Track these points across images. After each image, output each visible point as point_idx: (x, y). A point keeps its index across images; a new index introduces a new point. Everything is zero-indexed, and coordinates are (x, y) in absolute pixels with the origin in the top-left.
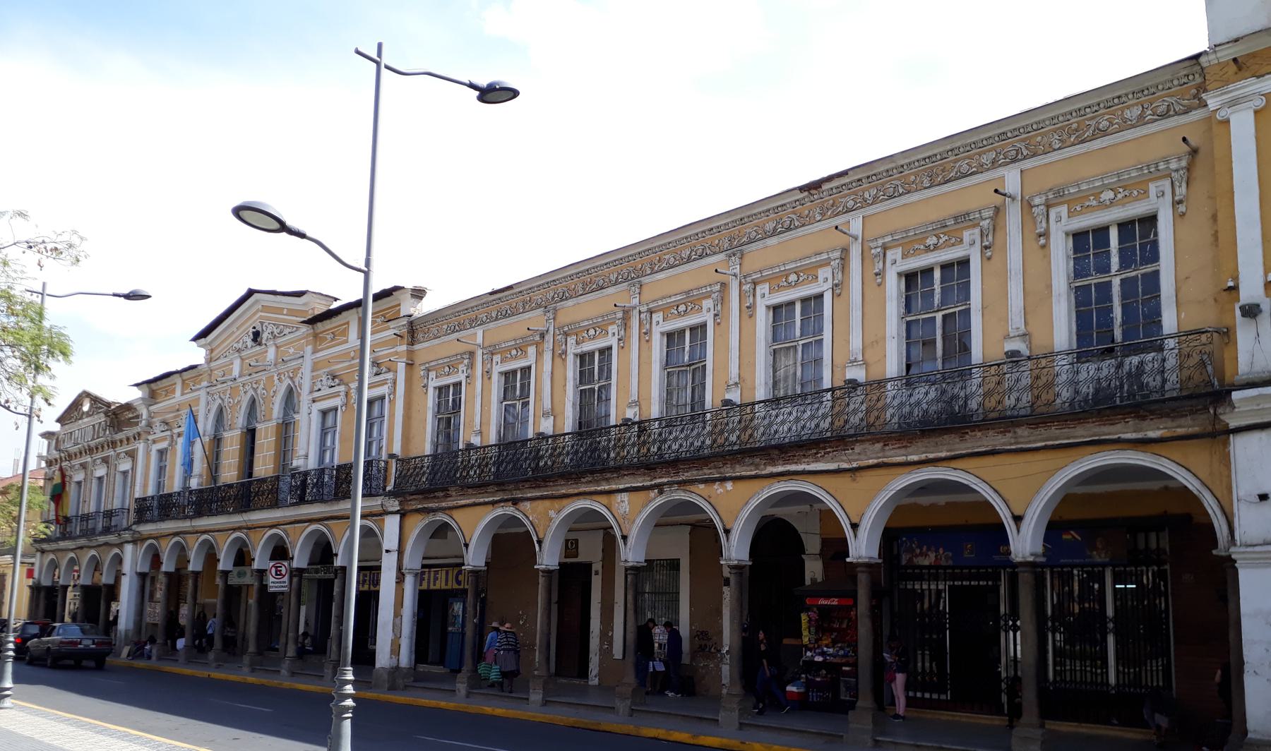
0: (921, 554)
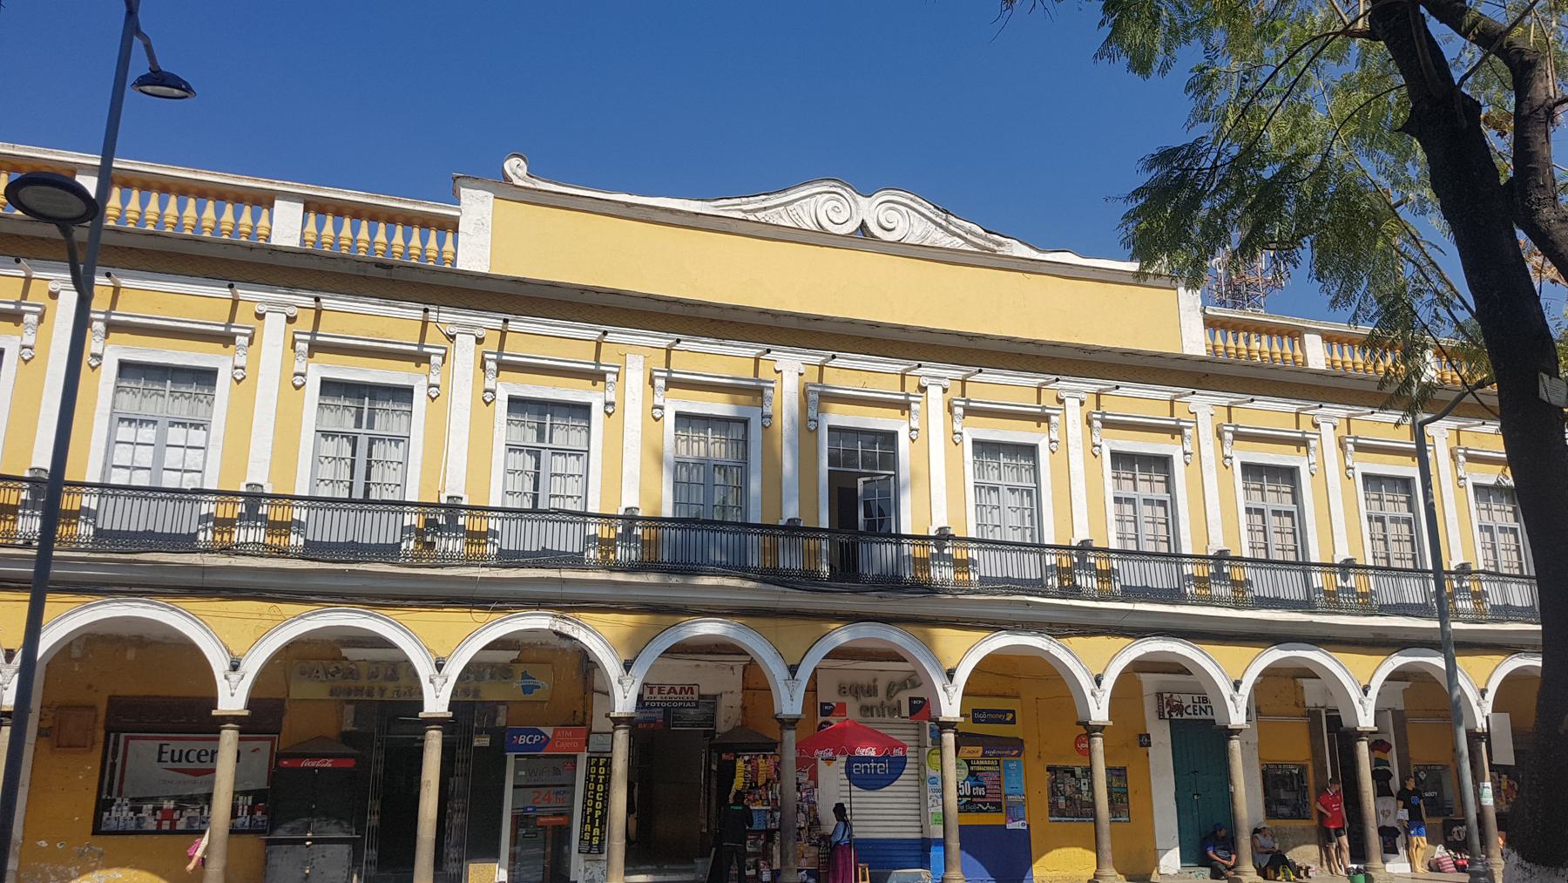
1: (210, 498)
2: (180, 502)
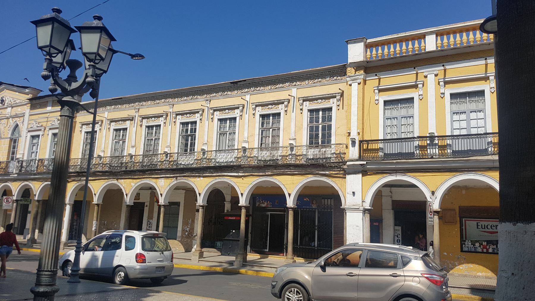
0: (262, 203)
1: (491, 136)
2: (480, 138)
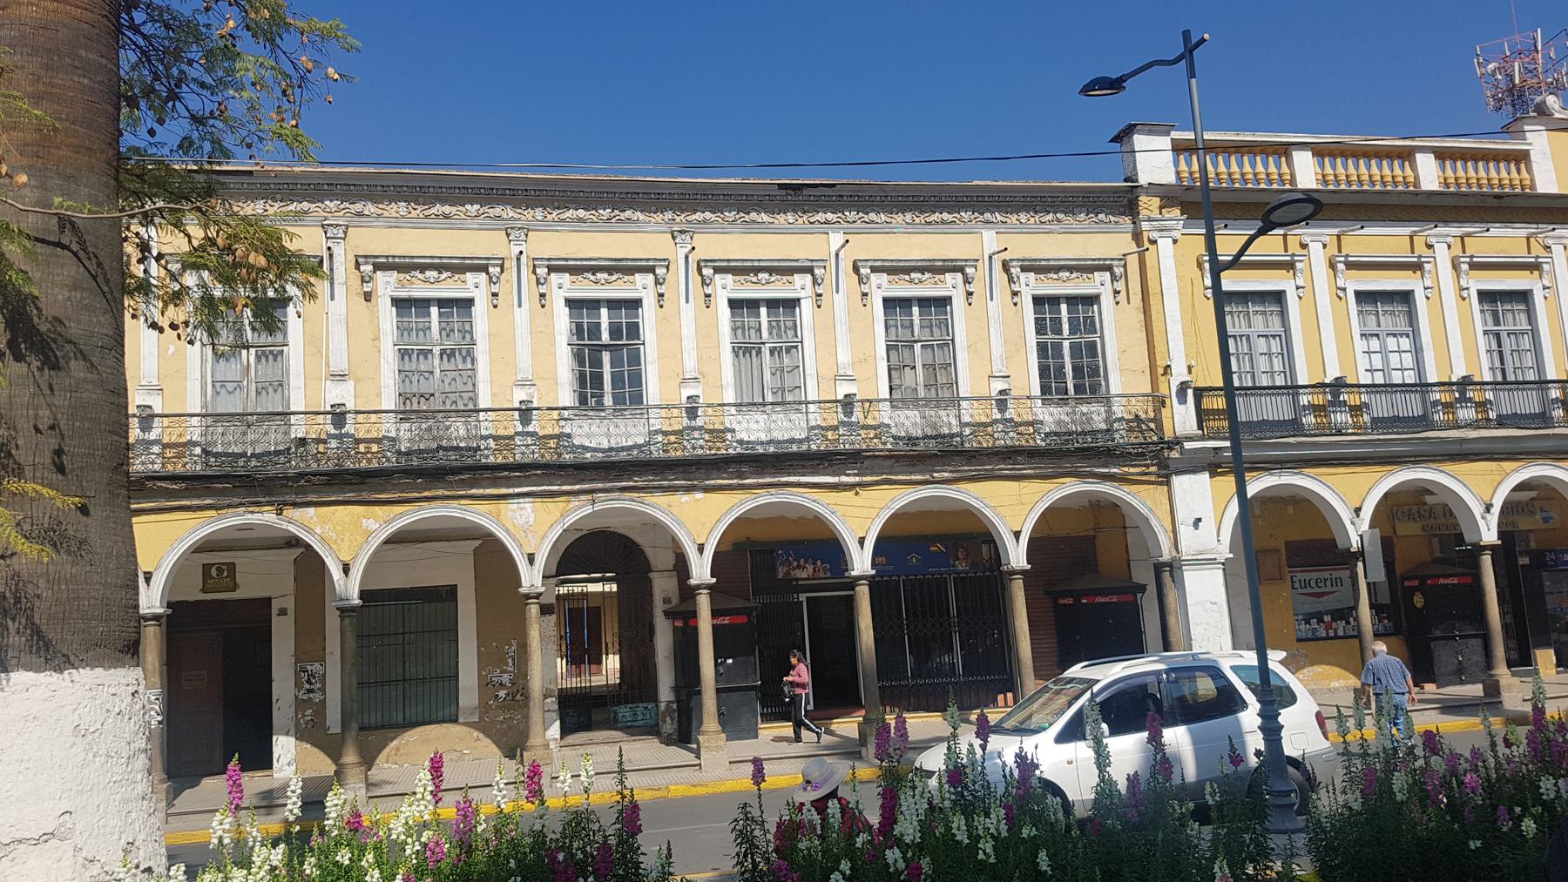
0: (799, 567)
